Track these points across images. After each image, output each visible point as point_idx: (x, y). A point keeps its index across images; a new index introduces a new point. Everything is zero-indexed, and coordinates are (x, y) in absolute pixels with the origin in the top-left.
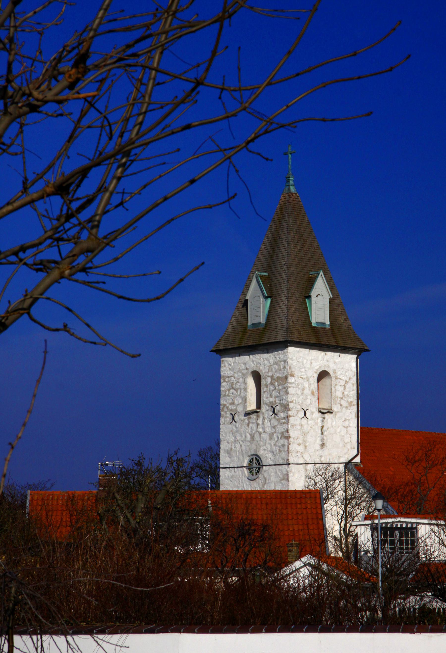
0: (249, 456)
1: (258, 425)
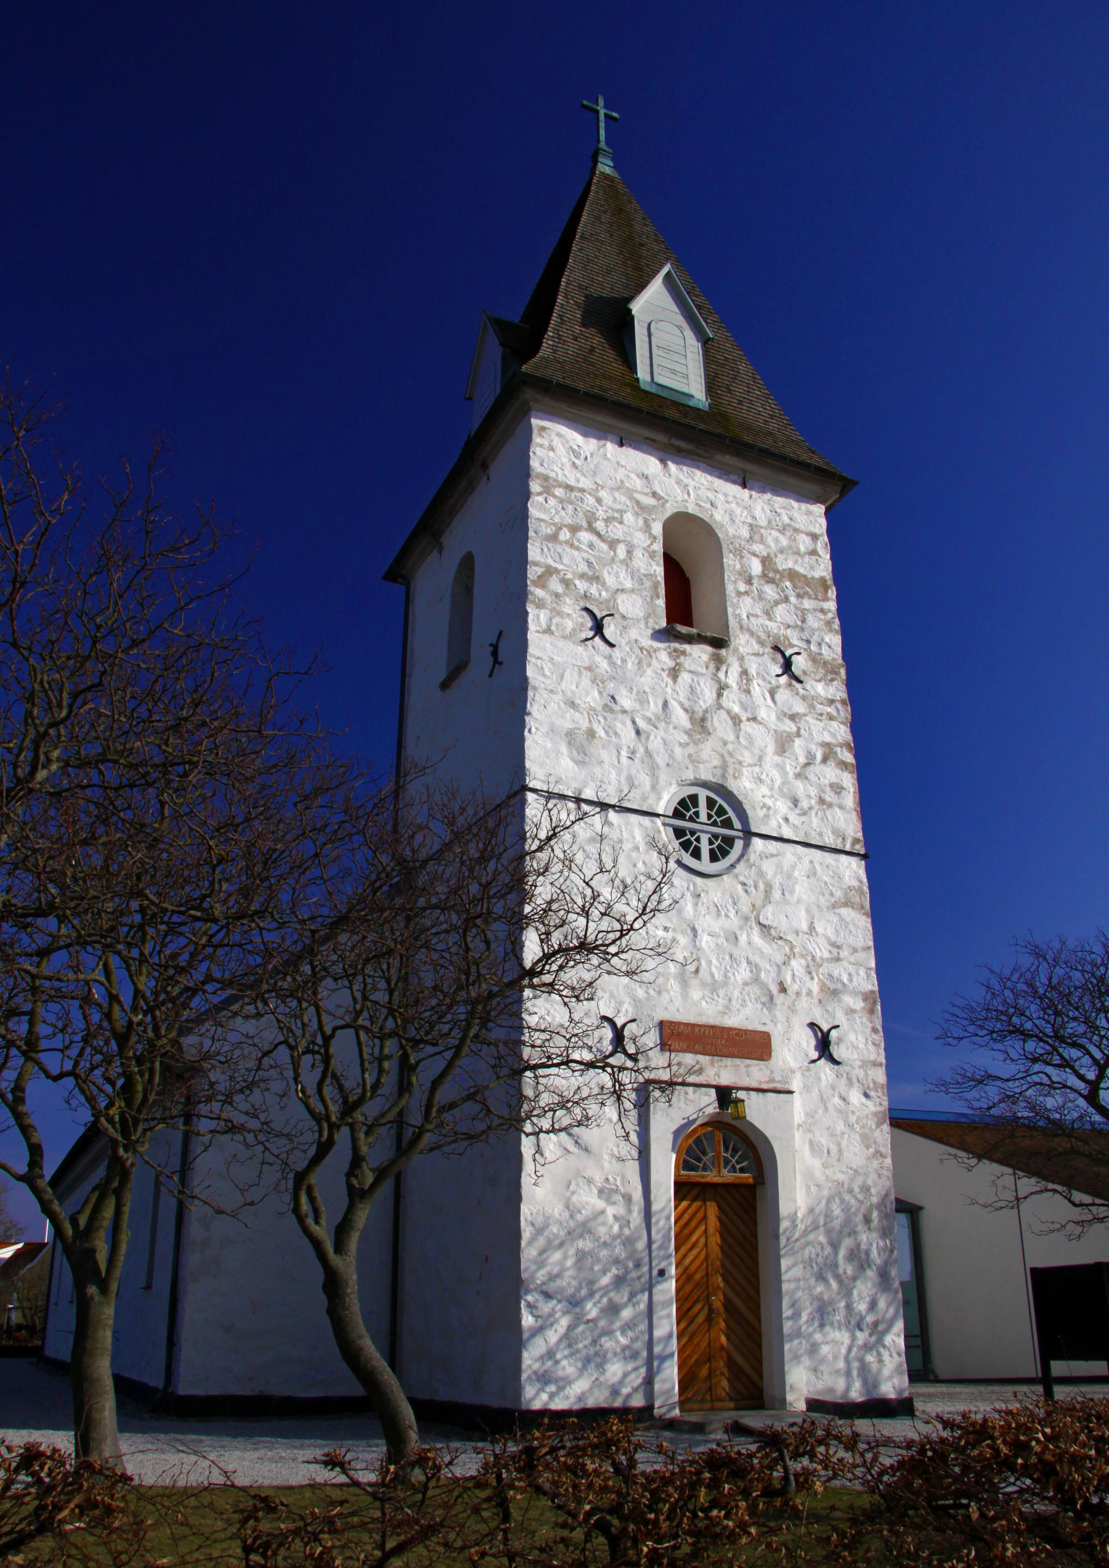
0: (682, 784)
1: (721, 688)
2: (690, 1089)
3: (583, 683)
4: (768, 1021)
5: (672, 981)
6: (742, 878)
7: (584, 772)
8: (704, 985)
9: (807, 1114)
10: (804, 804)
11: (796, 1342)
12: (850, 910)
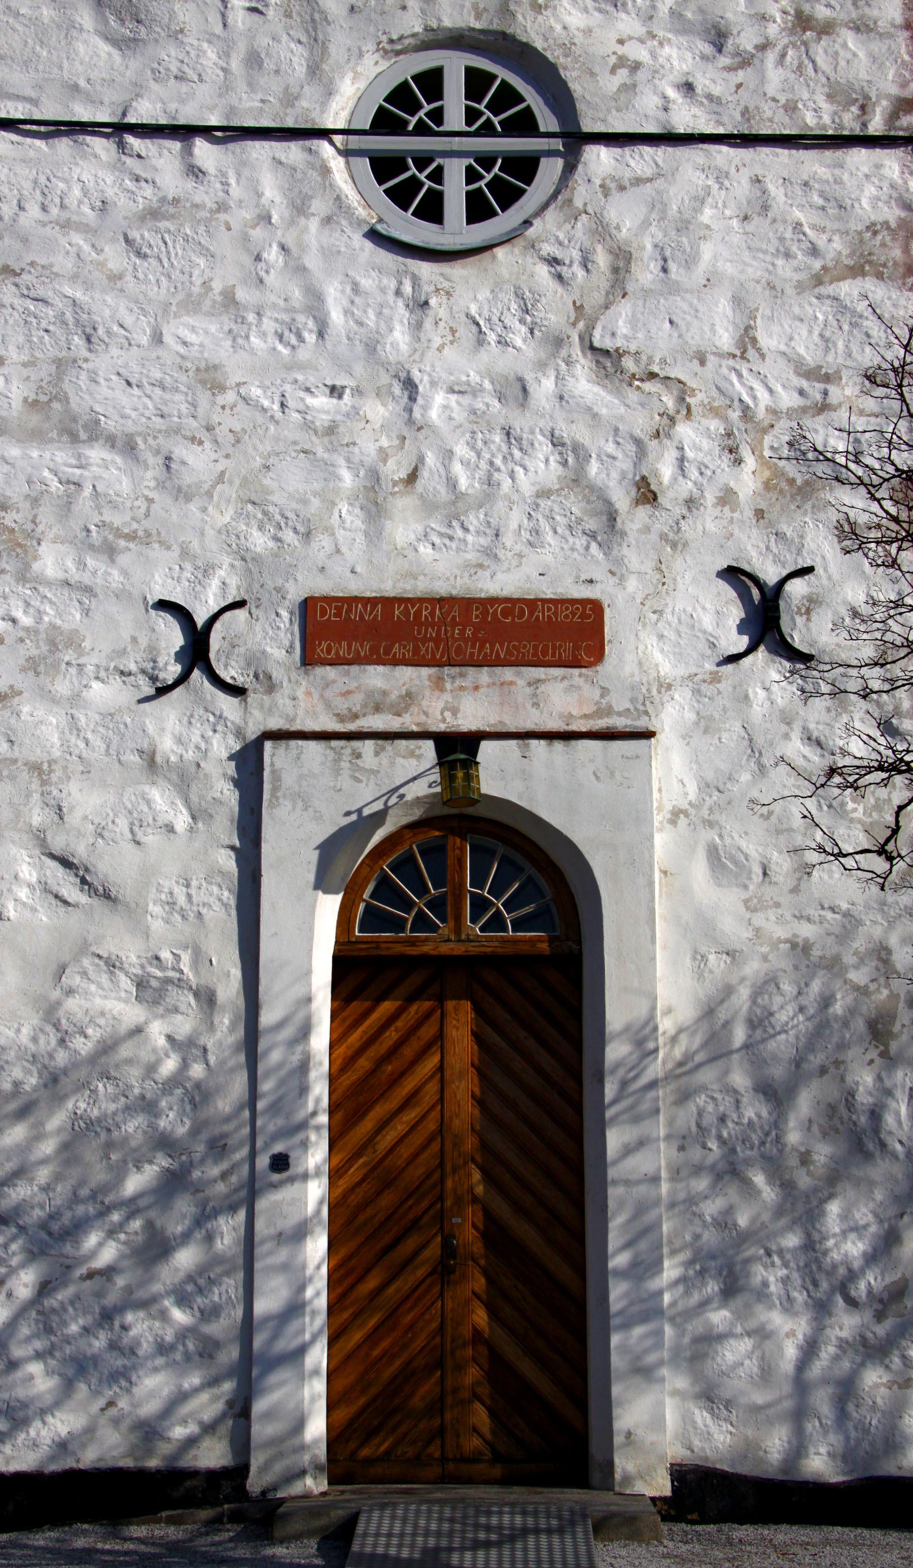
2: (369, 745)
4: (598, 574)
5: (345, 508)
6: (548, 249)
7: (134, 64)
8: (429, 506)
9: (705, 786)
10: (747, 40)
11: (638, 1331)
12: (869, 284)
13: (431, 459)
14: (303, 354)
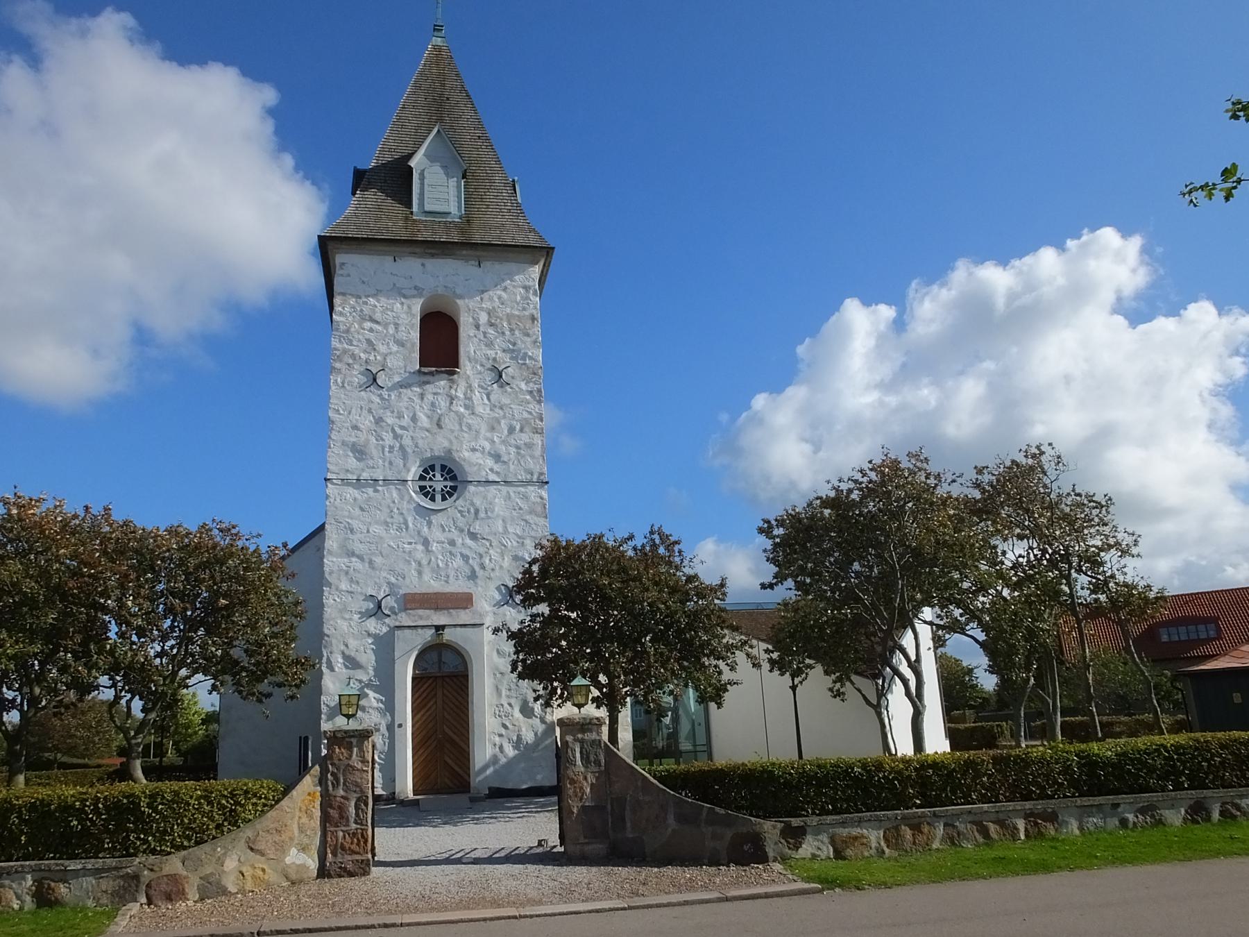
1: (452, 399)
3: (363, 414)
7: (362, 464)
13: (433, 559)
14: (403, 534)
